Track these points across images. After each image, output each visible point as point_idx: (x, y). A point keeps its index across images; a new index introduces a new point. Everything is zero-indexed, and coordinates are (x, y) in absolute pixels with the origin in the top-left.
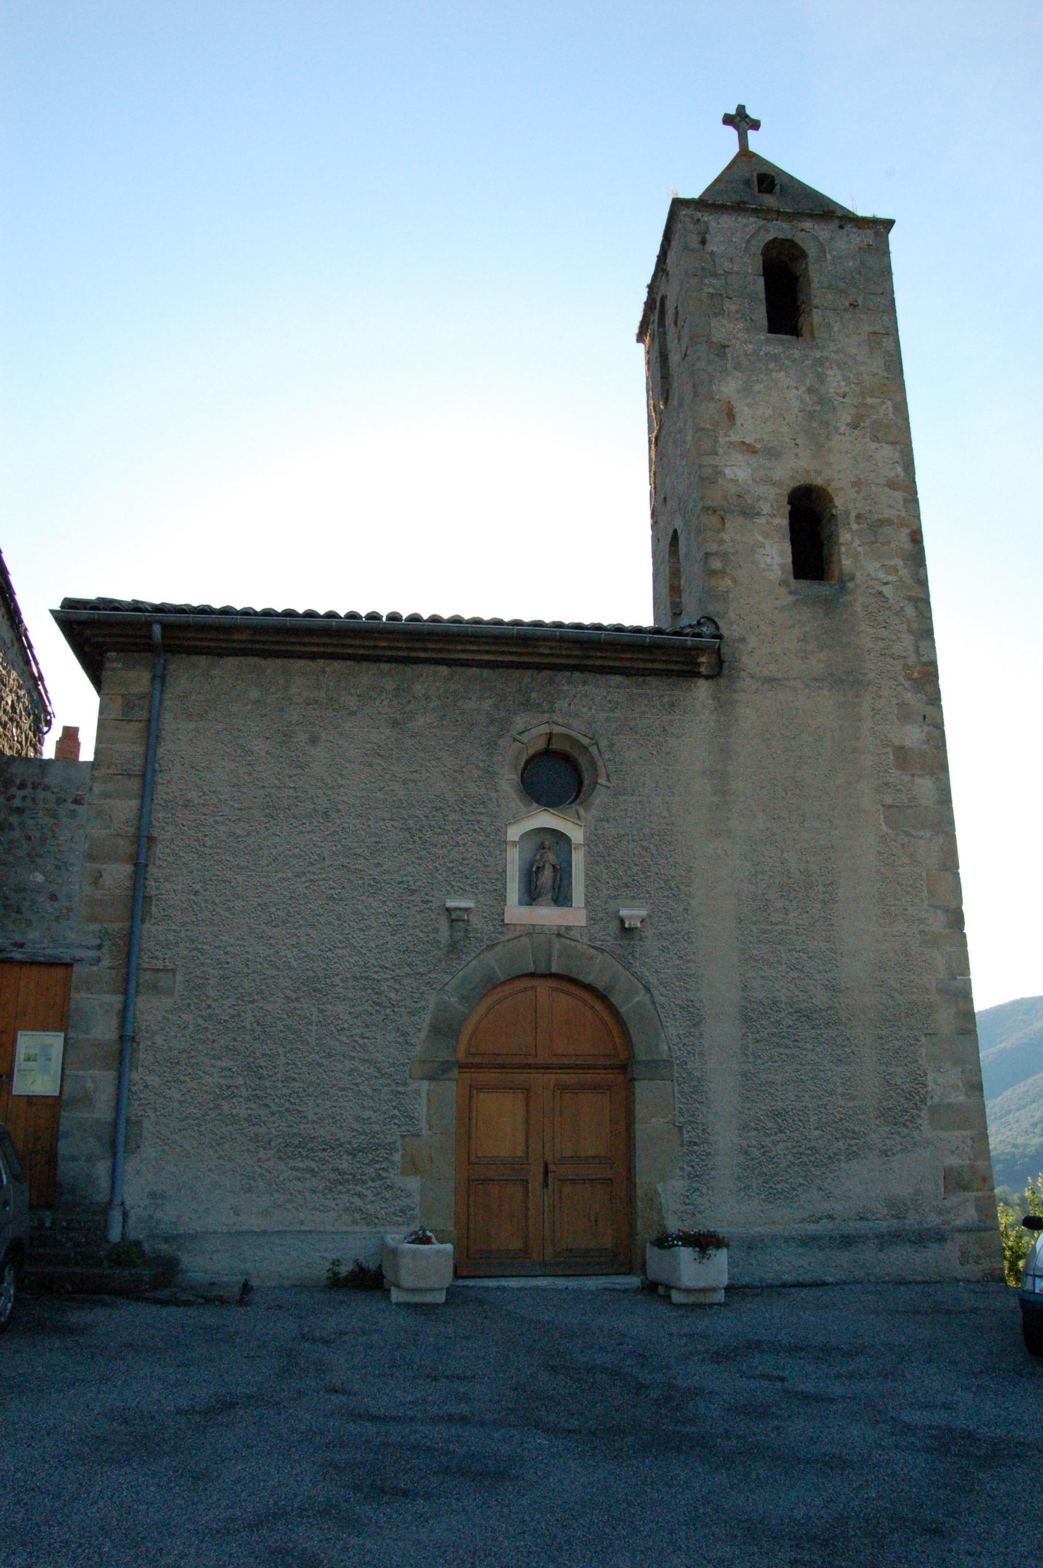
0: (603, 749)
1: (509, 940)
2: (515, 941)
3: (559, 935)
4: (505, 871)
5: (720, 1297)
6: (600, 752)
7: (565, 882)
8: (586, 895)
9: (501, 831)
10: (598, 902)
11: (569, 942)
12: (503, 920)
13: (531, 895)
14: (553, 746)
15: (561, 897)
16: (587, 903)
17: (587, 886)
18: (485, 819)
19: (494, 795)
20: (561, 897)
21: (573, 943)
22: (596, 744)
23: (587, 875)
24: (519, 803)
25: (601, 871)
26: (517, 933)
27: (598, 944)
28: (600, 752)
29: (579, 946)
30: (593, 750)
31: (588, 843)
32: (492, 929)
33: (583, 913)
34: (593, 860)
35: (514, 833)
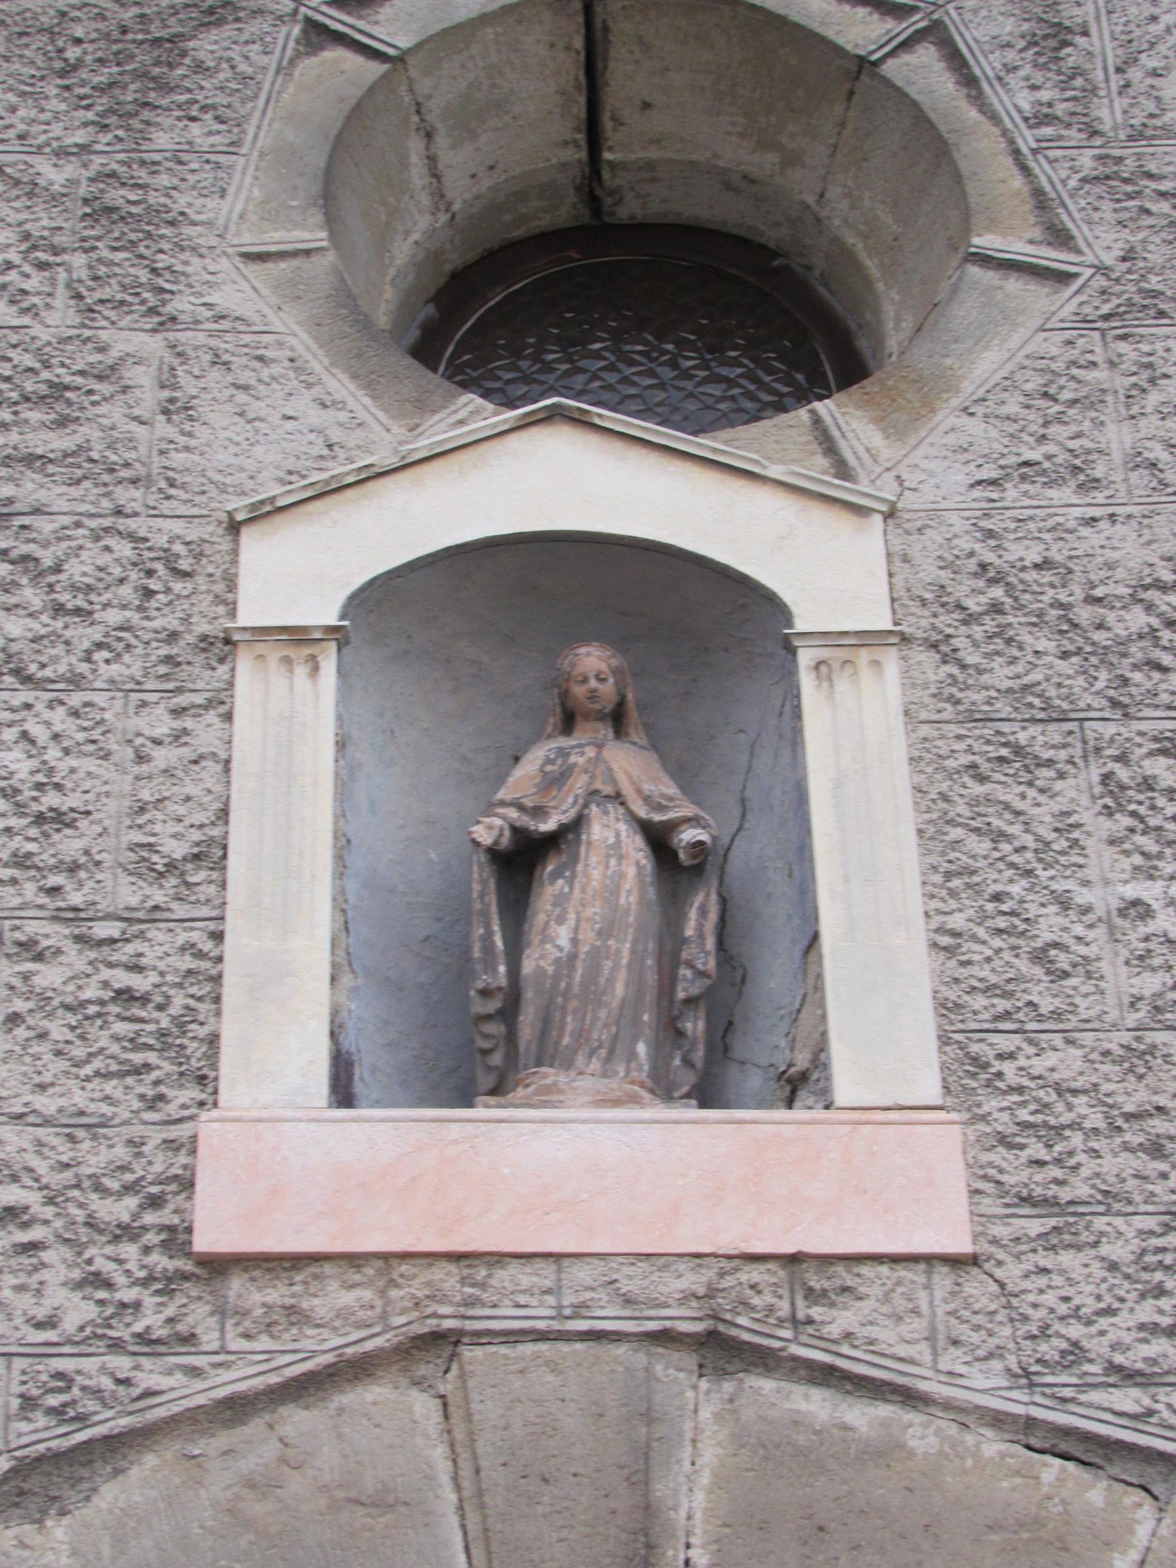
0: (986, 65)
1: (236, 1409)
2: (296, 1419)
3: (720, 1350)
4: (212, 855)
5: (466, 1340)
6: (969, 81)
7: (773, 976)
8: (946, 1008)
9: (191, 568)
10: (1065, 1063)
11: (816, 1404)
12: (176, 1238)
13: (466, 1036)
14: (929, 1089)
15: (721, 1032)
16: (969, 1072)
17: (947, 944)
18: (57, 496)
19: (130, 339)
20: (721, 1032)
21: (862, 1416)
22: (936, 33)
23: (948, 877)
24: (340, 385)
25: (1066, 825)
26: (319, 1347)
27: (1107, 1410)
28: (969, 81)
29: (921, 1434)
30: (922, 74)
31: (933, 629)
32: (79, 1312)
33: (944, 1148)
34: (981, 762)
35: (301, 573)
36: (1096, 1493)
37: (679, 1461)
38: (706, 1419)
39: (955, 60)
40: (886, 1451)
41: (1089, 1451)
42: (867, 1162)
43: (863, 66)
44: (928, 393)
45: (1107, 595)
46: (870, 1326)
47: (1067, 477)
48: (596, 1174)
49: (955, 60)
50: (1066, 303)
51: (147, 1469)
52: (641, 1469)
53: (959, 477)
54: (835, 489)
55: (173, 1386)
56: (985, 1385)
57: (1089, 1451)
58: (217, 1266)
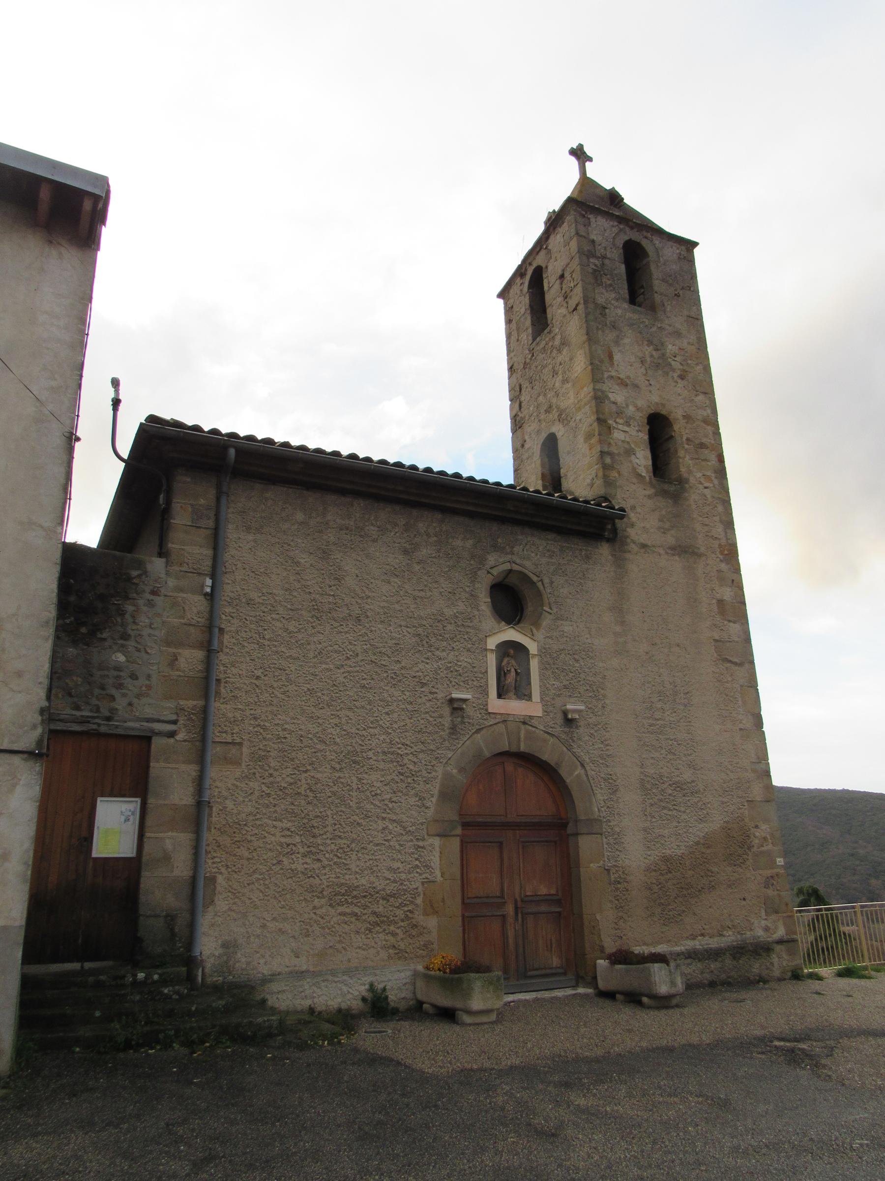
2: (495, 726)
3: (524, 723)
4: (486, 672)
11: (530, 728)
12: (487, 710)
17: (540, 686)
22: (541, 580)
30: (539, 584)
31: (543, 652)
33: (540, 705)
34: (544, 667)
35: (492, 643)
36: (548, 737)
37: (526, 721)
38: (523, 727)
39: (543, 584)
40: (535, 732)
41: (548, 733)
42: (532, 708)
43: (534, 583)
44: (536, 624)
45: (441, 869)
46: (534, 722)
47: (770, 892)
48: (514, 707)
49: (543, 584)
50: (551, 617)
51: (485, 730)
52: (519, 733)
53: (542, 637)
54: (532, 637)
55: (487, 723)
56: (542, 728)
57: (548, 733)
58: (490, 713)
